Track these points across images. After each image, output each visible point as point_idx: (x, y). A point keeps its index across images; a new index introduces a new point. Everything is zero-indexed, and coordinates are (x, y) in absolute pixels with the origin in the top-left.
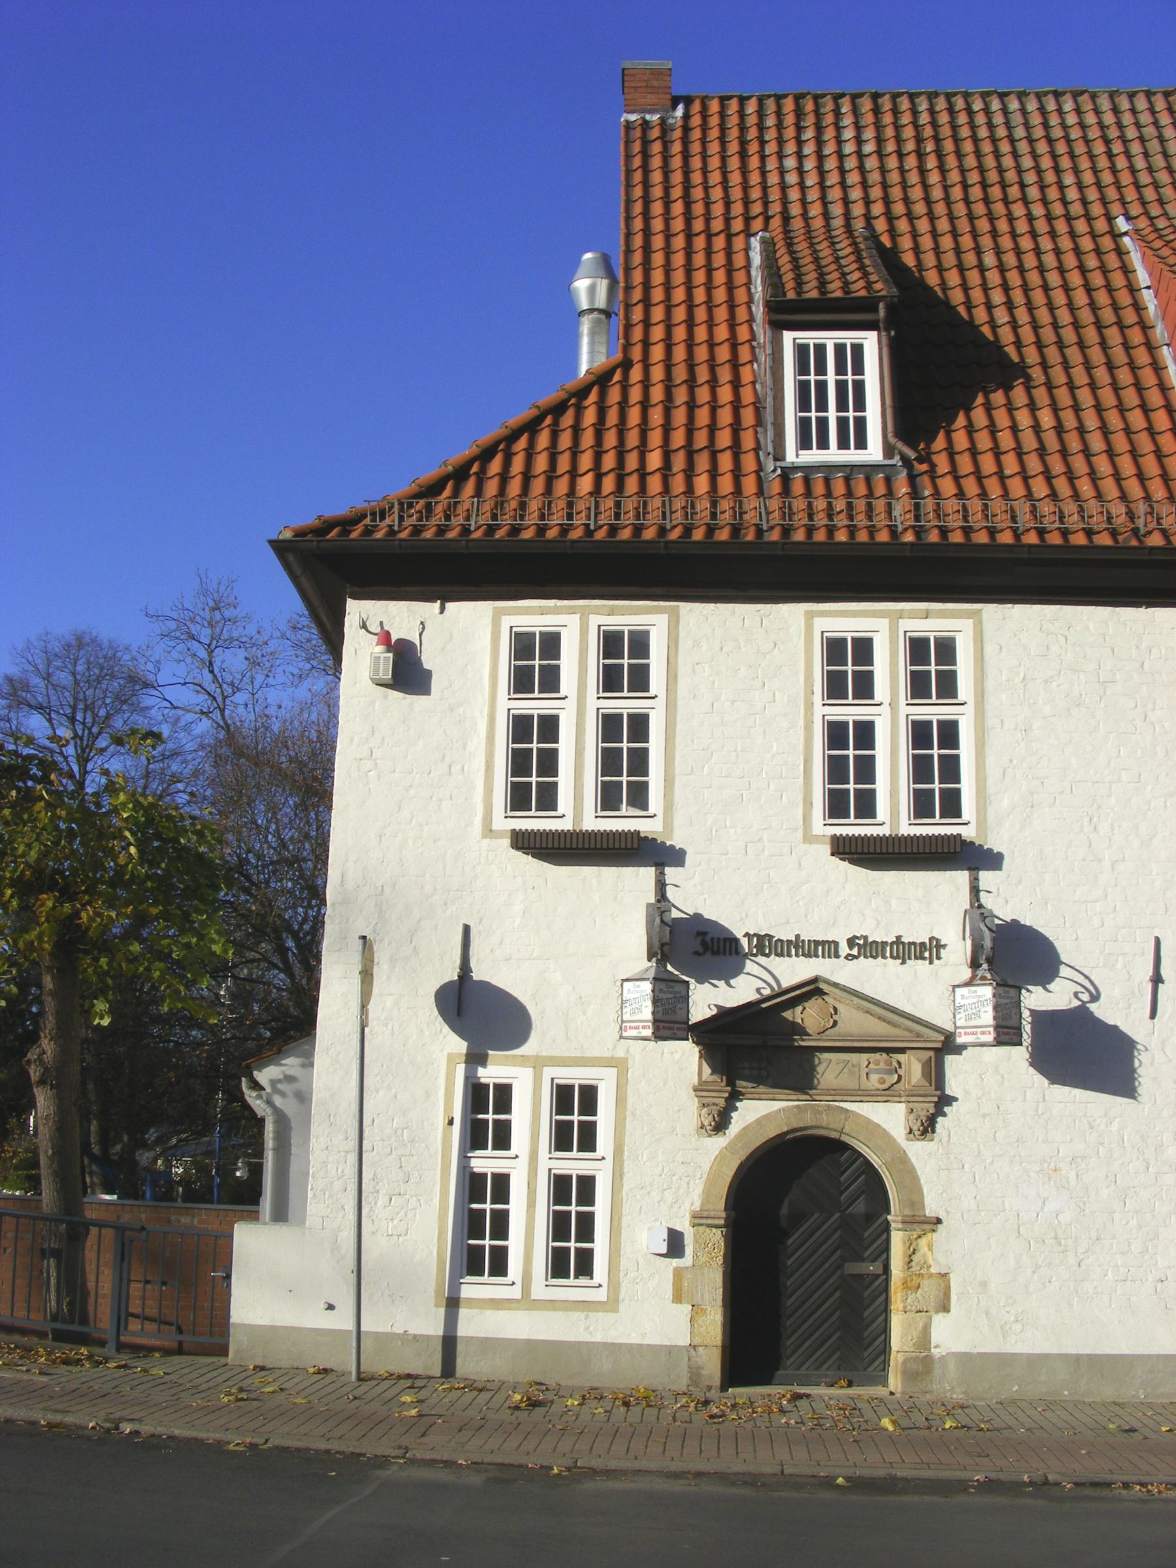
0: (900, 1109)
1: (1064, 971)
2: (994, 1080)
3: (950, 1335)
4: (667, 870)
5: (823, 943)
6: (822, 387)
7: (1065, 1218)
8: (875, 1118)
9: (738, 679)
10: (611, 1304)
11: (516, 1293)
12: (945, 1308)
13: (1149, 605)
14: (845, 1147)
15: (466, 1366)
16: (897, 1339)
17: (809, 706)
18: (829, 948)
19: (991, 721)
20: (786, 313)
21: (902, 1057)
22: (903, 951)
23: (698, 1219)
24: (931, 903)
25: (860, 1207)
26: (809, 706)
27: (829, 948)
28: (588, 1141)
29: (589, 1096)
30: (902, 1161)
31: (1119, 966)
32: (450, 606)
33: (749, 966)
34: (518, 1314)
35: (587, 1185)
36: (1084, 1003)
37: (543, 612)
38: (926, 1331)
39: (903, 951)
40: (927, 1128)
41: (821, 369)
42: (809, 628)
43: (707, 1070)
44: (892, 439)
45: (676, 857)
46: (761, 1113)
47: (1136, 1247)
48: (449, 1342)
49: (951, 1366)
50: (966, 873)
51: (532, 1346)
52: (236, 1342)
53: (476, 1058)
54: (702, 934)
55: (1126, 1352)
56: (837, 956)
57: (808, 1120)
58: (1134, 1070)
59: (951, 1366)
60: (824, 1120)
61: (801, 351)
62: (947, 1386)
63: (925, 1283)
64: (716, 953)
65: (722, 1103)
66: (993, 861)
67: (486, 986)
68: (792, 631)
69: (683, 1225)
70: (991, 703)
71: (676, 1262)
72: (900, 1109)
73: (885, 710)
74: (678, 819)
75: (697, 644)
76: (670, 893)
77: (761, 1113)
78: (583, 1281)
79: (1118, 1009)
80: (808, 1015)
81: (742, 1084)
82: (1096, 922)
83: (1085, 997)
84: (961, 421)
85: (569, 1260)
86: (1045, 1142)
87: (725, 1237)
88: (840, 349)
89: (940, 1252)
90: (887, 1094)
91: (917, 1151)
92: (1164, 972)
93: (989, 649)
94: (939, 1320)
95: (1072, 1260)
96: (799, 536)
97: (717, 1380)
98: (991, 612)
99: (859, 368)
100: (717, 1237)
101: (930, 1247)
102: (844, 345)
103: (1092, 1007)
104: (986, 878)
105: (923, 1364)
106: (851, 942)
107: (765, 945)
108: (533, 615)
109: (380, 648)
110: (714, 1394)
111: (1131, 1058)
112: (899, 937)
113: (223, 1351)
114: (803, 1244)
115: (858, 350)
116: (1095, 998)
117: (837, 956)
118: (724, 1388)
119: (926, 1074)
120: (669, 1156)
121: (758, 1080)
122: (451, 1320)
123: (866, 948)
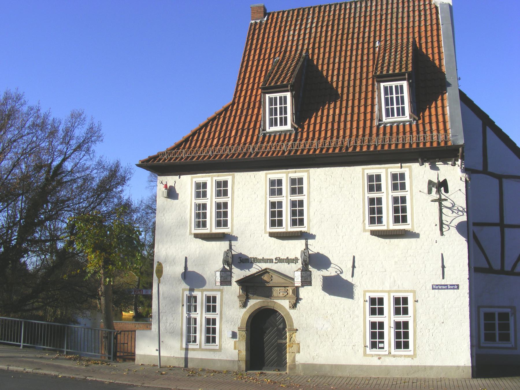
0: (287, 301)
1: (332, 265)
2: (313, 295)
3: (301, 358)
4: (232, 242)
5: (269, 259)
6: (392, 98)
7: (329, 329)
8: (282, 304)
9: (249, 192)
10: (220, 350)
11: (198, 347)
12: (299, 352)
13: (354, 166)
14: (277, 312)
15: (190, 365)
16: (288, 360)
17: (266, 198)
18: (271, 261)
19: (312, 200)
20: (267, 89)
21: (288, 288)
22: (288, 261)
23: (239, 329)
24: (294, 249)
25: (281, 326)
26: (266, 198)
27: (271, 261)
28: (214, 310)
29: (214, 298)
30: (288, 314)
31: (344, 263)
32: (181, 176)
33: (254, 266)
34: (200, 353)
35: (214, 320)
36: (338, 274)
37: (202, 177)
38: (294, 357)
39: (288, 261)
40: (294, 306)
41: (391, 93)
42: (266, 177)
43: (241, 291)
44: (411, 114)
45: (235, 239)
46: (254, 303)
47: (347, 337)
48: (186, 359)
49: (300, 366)
50: (304, 240)
51: (202, 360)
52: (137, 358)
53: (191, 290)
54: (240, 258)
55: (344, 363)
56: (273, 262)
57: (265, 304)
58: (353, 292)
59: (300, 366)
60: (270, 304)
61: (386, 88)
62: (300, 371)
63: (294, 345)
64: (243, 262)
65: (244, 300)
66: (313, 237)
67: (194, 272)
68: (261, 179)
69: (236, 330)
70: (312, 195)
71: (234, 340)
72: (287, 301)
73: (285, 198)
74: (235, 229)
75: (239, 183)
76: (233, 247)
77: (254, 303)
78: (214, 344)
79: (346, 276)
80: (265, 278)
81: (250, 295)
82: (338, 252)
83: (339, 272)
84: (433, 105)
85: (210, 339)
86: (324, 310)
87: (246, 334)
88: (396, 87)
89: (298, 337)
90: (285, 297)
91: (293, 313)
92: (356, 265)
93: (311, 180)
94: (297, 355)
95: (331, 340)
96: (421, 146)
97: (244, 369)
98: (312, 170)
99: (402, 92)
100: (244, 333)
101: (295, 336)
102: (277, 97)
103: (341, 275)
104: (310, 241)
105: (294, 366)
106: (276, 259)
107: (256, 260)
108: (200, 178)
109: (164, 189)
110: (245, 373)
111: (352, 289)
112: (287, 258)
113: (134, 360)
114: (266, 336)
115: (402, 87)
116: (342, 273)
117: (273, 262)
118: (246, 371)
119: (293, 292)
120: (233, 313)
121: (254, 294)
122: (186, 354)
123: (279, 260)
